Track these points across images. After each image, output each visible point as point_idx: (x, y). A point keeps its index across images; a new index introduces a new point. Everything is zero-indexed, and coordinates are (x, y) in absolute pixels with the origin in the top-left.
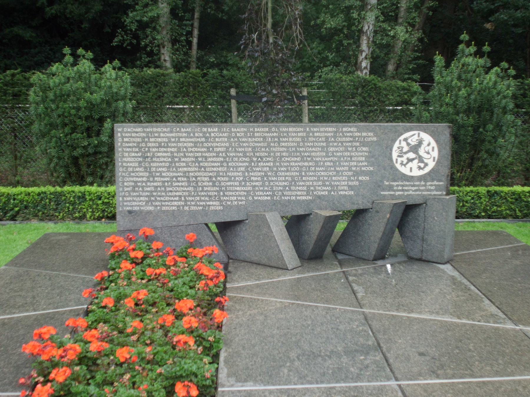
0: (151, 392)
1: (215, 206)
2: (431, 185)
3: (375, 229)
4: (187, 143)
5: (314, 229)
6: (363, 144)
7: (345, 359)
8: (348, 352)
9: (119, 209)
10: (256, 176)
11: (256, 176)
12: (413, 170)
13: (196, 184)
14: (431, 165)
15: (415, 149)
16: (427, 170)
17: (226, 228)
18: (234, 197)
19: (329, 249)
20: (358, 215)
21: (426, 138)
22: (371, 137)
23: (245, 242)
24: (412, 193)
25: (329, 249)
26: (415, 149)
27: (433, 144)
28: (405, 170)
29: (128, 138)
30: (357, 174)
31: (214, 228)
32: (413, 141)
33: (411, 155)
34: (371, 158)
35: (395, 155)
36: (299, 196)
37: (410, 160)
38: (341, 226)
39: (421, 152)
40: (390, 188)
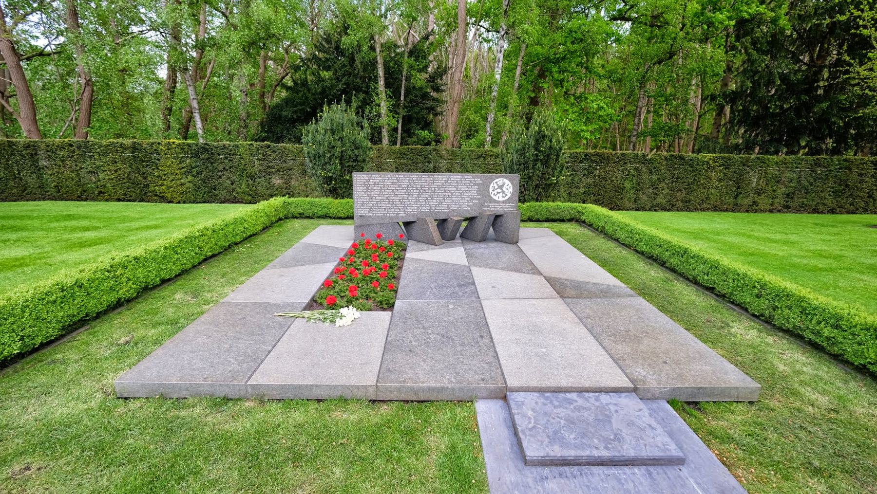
0: (727, 147)
1: (402, 214)
2: (509, 205)
3: (480, 225)
4: (388, 183)
5: (450, 226)
6: (475, 184)
7: (457, 289)
8: (460, 286)
9: (355, 215)
10: (422, 199)
11: (422, 199)
12: (500, 198)
13: (392, 202)
14: (509, 195)
15: (501, 187)
16: (507, 198)
17: (407, 224)
18: (411, 211)
19: (458, 235)
20: (471, 219)
21: (507, 181)
22: (479, 181)
23: (416, 229)
24: (499, 209)
25: (458, 235)
26: (501, 187)
27: (510, 185)
28: (496, 198)
29: (359, 178)
30: (471, 199)
31: (401, 224)
32: (500, 183)
33: (499, 190)
34: (479, 192)
35: (491, 190)
36: (443, 210)
37: (498, 193)
38: (464, 224)
39: (504, 189)
40: (488, 206)
